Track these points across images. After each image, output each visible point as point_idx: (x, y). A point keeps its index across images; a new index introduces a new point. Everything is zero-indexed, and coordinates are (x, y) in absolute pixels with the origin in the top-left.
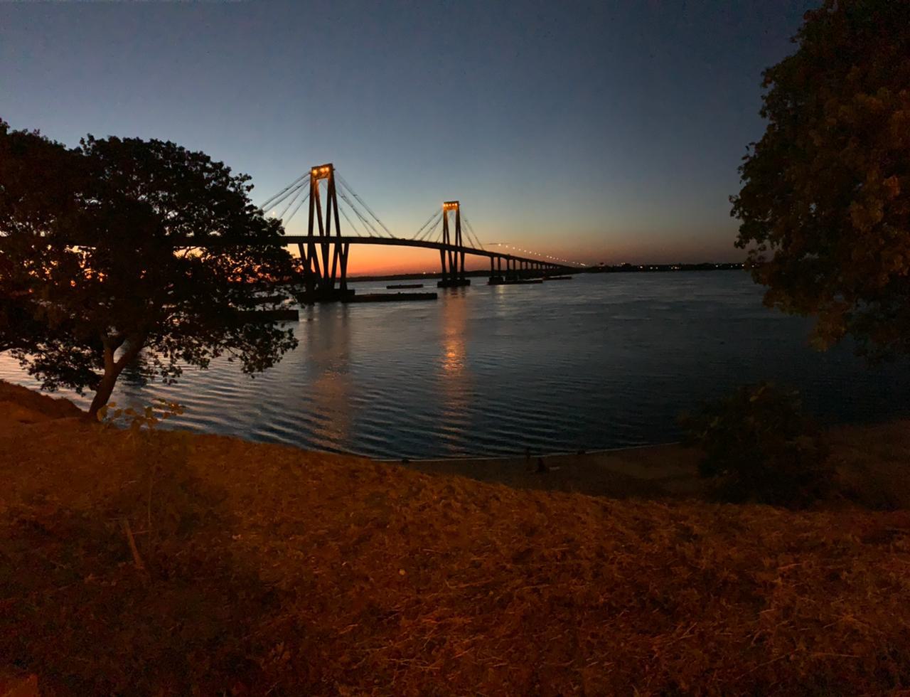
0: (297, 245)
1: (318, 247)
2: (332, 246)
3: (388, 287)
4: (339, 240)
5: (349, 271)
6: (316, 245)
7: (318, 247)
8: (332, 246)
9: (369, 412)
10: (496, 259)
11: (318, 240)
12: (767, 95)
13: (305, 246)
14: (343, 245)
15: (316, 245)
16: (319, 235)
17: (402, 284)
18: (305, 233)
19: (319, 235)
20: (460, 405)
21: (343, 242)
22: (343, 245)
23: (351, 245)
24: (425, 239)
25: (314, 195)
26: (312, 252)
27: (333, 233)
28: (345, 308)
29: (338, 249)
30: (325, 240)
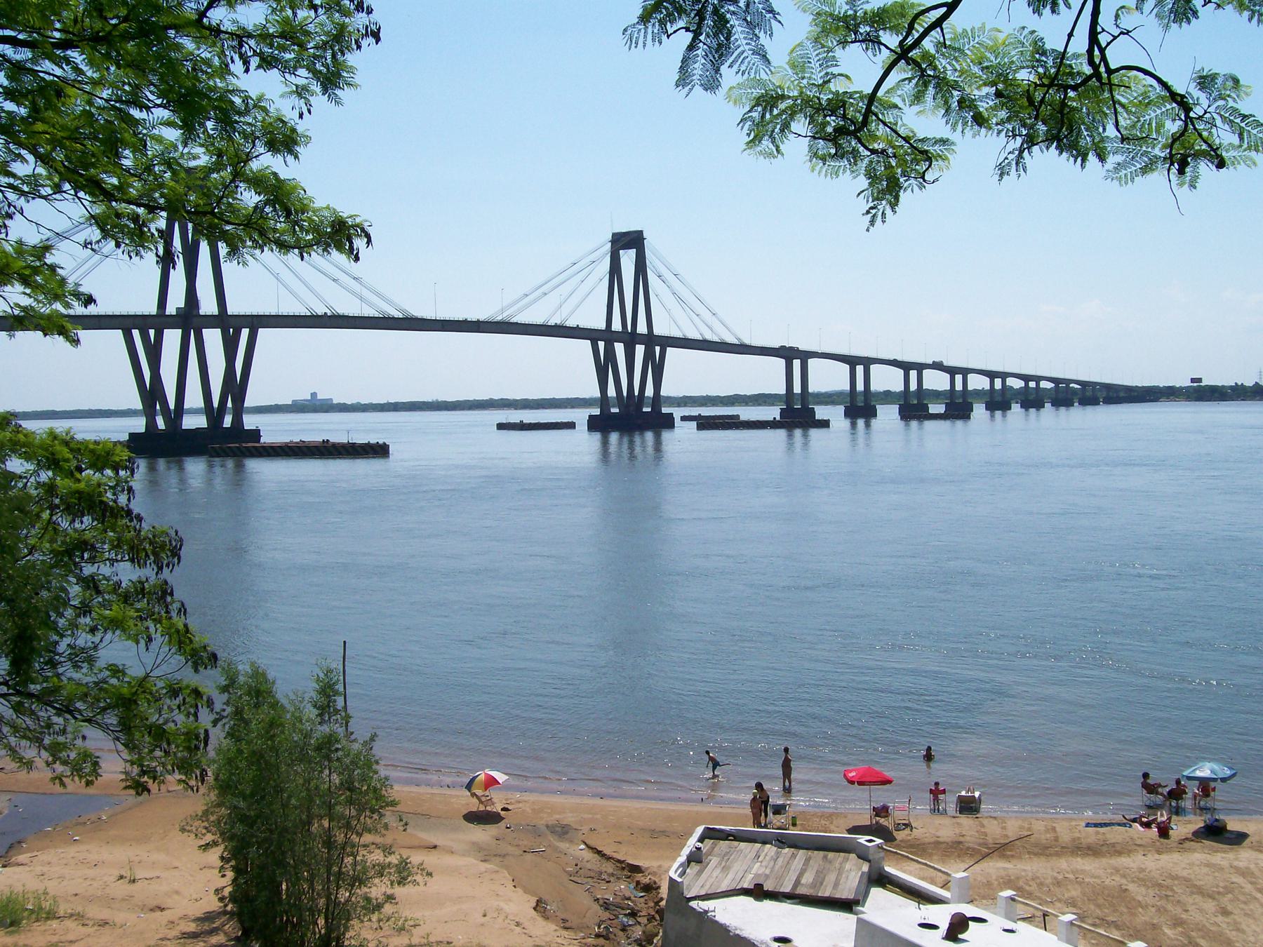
0: (219, 331)
1: (619, 348)
2: (640, 350)
3: (379, 451)
4: (651, 340)
5: (664, 392)
6: (133, 331)
7: (619, 348)
8: (640, 350)
9: (674, 664)
10: (959, 378)
11: (618, 337)
12: (152, 781)
13: (601, 344)
14: (658, 349)
15: (133, 331)
16: (216, 312)
17: (743, 418)
18: (153, 310)
19: (216, 312)
20: (1047, 689)
21: (657, 344)
22: (658, 349)
23: (670, 351)
24: (571, 323)
25: (615, 270)
26: (611, 355)
27: (642, 328)
28: (805, 436)
29: (649, 355)
30: (631, 340)
